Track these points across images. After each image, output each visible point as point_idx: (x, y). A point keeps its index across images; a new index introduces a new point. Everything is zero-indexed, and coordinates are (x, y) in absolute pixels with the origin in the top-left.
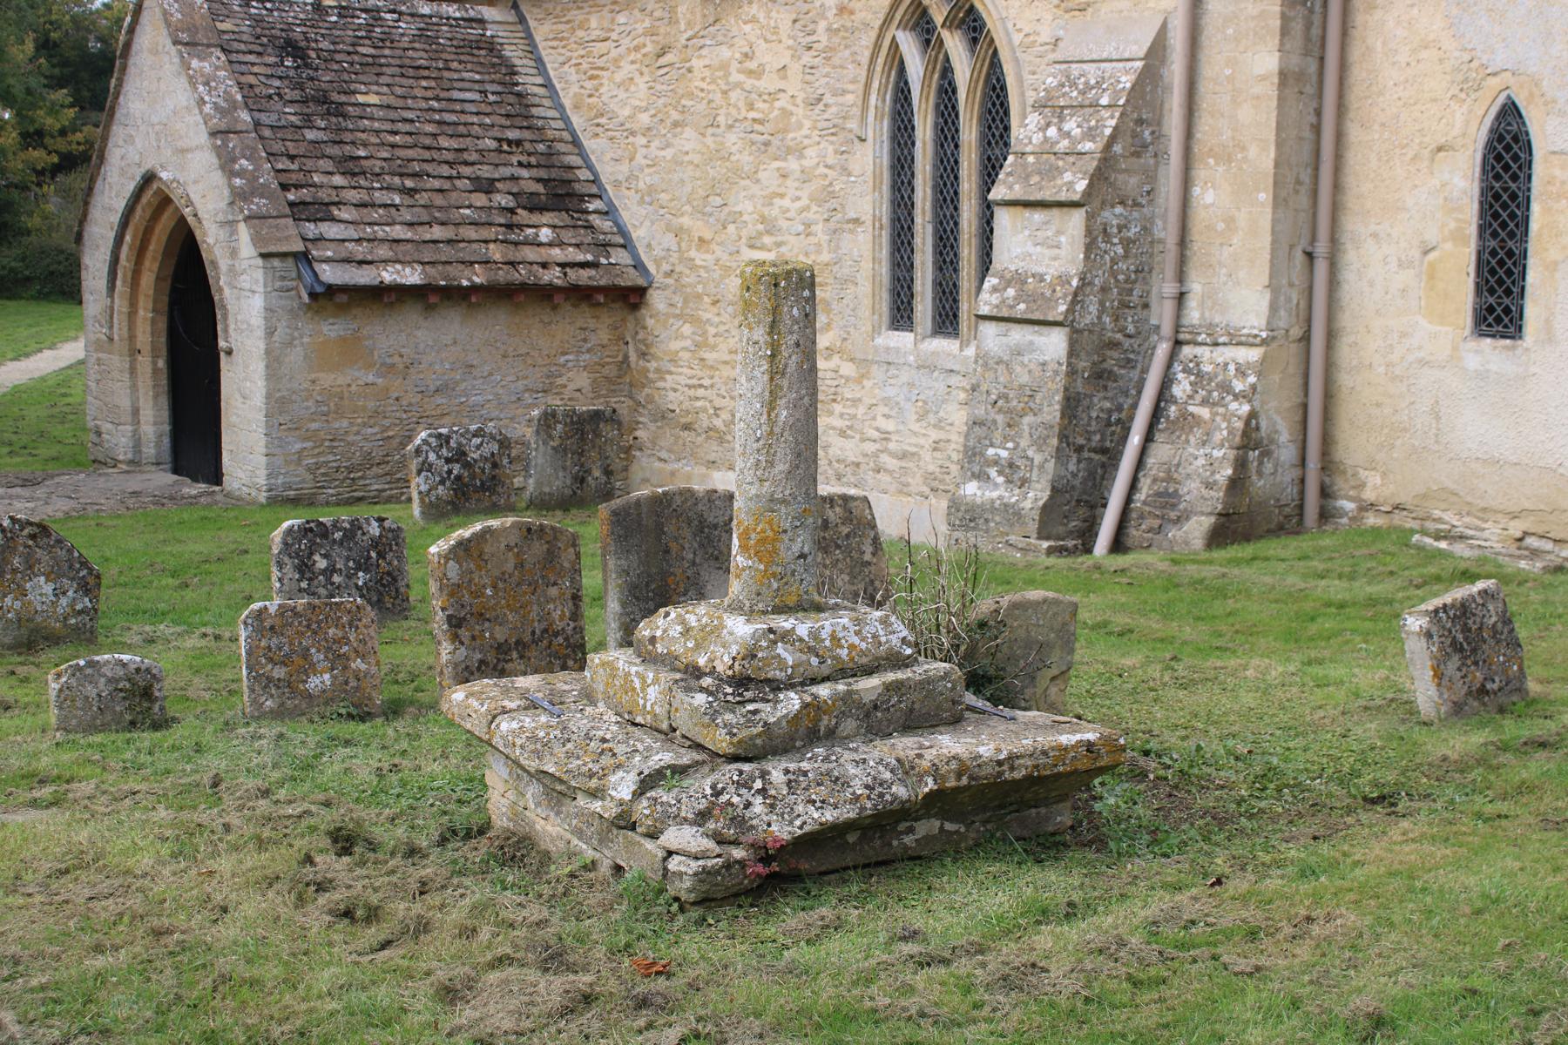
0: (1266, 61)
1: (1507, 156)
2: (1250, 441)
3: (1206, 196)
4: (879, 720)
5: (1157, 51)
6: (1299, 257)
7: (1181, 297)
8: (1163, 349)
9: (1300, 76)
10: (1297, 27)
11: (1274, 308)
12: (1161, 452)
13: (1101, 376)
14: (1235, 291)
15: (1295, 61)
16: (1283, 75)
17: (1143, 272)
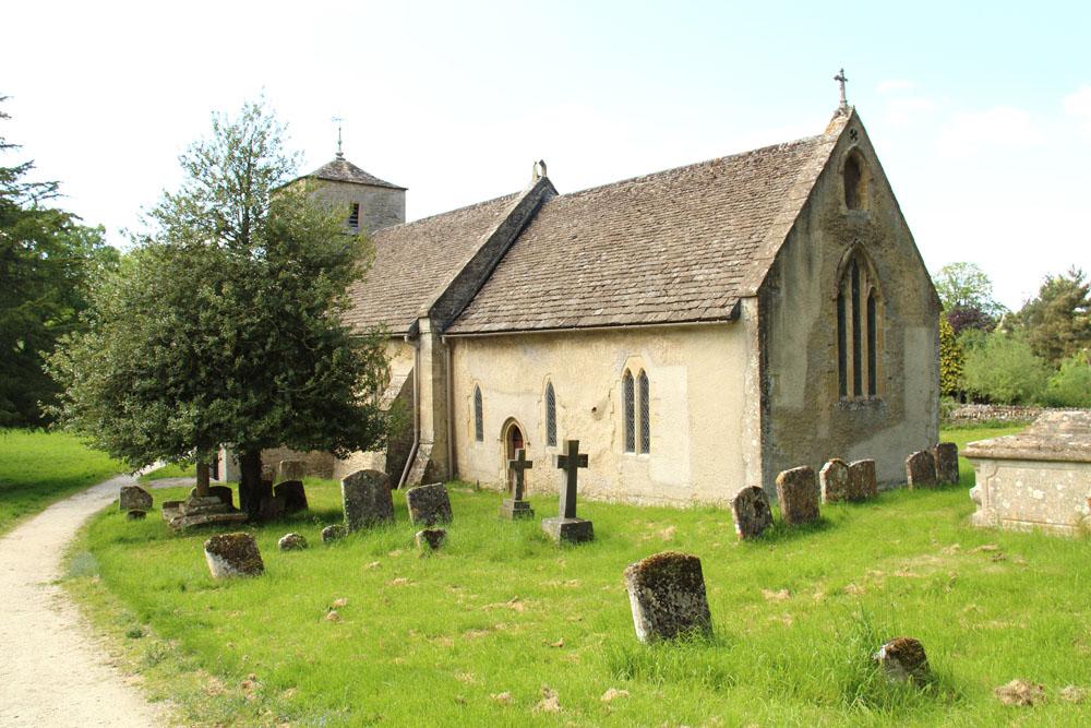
0: (430, 377)
1: (478, 399)
2: (430, 465)
3: (423, 408)
4: (210, 512)
5: (411, 374)
6: (444, 422)
7: (419, 433)
8: (415, 445)
9: (440, 380)
10: (438, 368)
11: (435, 435)
12: (413, 469)
13: (399, 452)
14: (428, 430)
15: (438, 376)
16: (434, 380)
17: (412, 426)
